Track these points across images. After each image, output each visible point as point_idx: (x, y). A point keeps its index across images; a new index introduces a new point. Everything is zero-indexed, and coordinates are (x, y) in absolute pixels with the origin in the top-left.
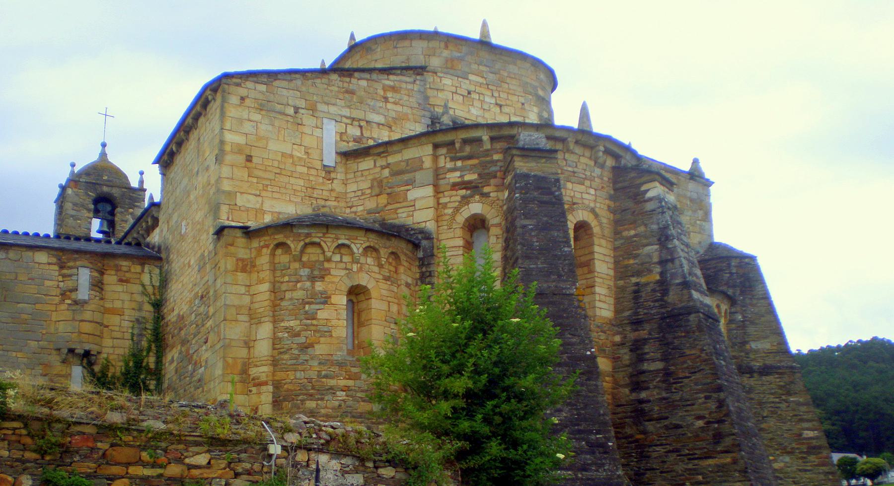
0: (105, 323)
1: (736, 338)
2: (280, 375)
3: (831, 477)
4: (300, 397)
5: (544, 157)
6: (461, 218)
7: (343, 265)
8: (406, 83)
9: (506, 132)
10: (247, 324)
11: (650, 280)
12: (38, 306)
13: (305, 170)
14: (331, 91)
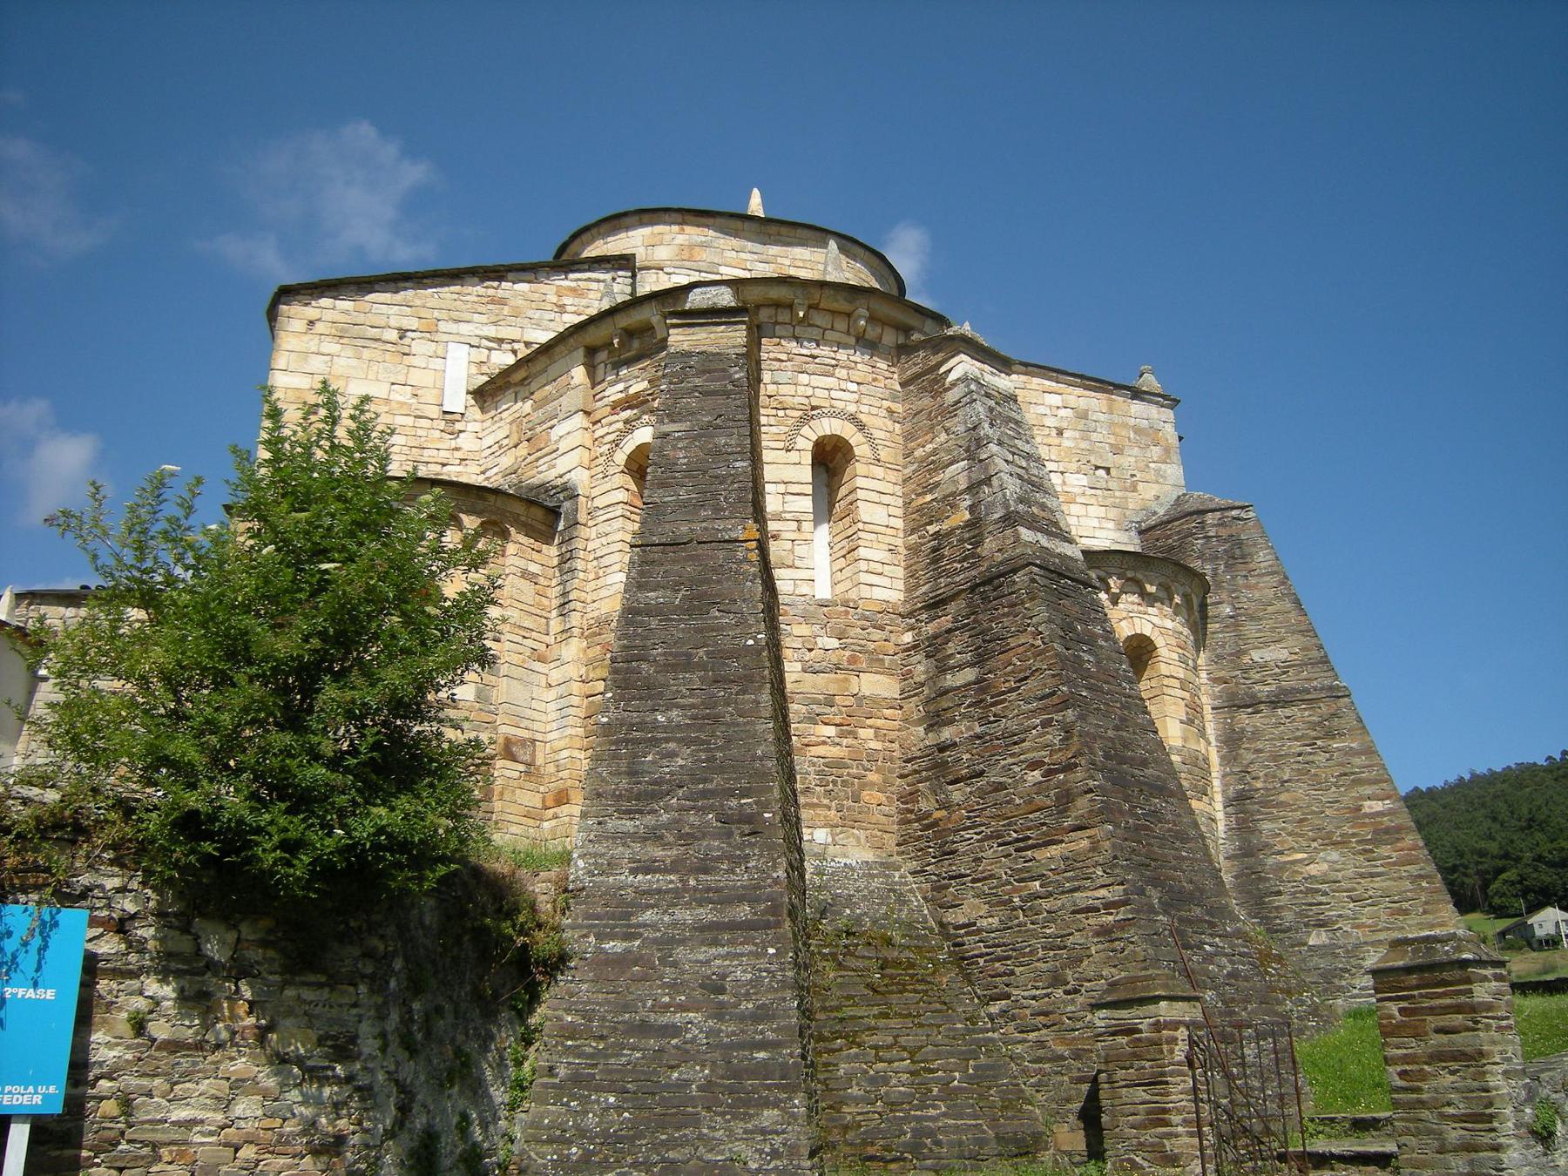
1: (1223, 647)
6: (621, 457)
13: (410, 421)
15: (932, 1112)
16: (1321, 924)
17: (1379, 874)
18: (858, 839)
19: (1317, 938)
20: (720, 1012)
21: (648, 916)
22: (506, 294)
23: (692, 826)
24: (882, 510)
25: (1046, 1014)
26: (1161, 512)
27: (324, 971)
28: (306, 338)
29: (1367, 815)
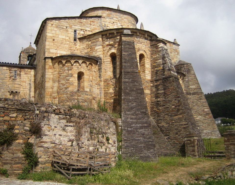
0: (21, 85)
2: (60, 96)
4: (65, 102)
6: (109, 54)
7: (77, 66)
8: (96, 20)
9: (121, 31)
10: (52, 82)
11: (160, 69)
12: (4, 80)
13: (69, 43)
20: (144, 138)
21: (133, 125)
22: (82, 21)
24: (148, 65)
25: (175, 138)
26: (177, 63)
28: (51, 27)
29: (205, 111)
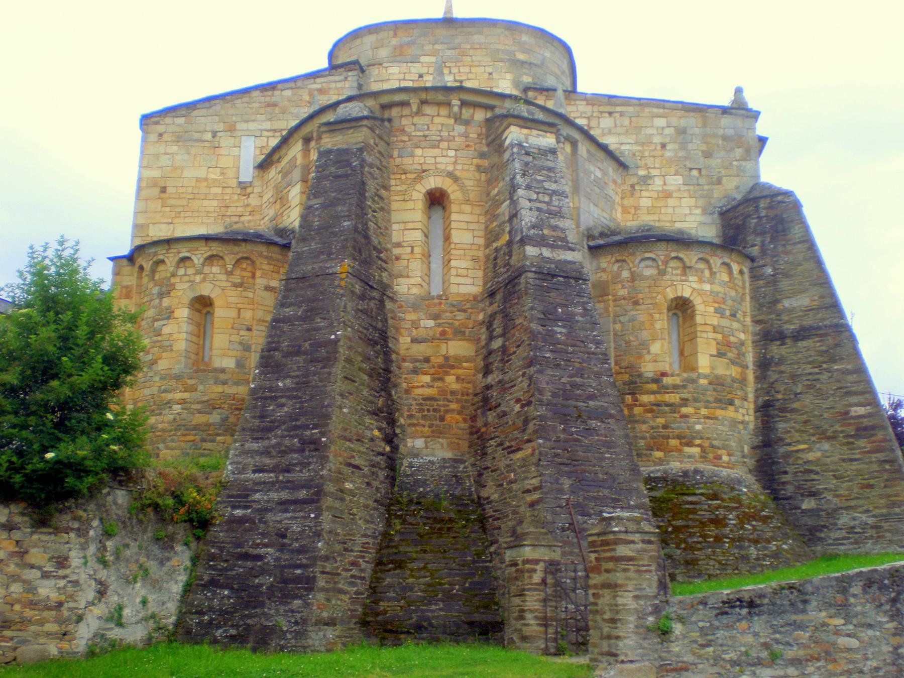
3: (887, 467)
5: (351, 128)
8: (336, 82)
13: (219, 190)
14: (252, 108)
15: (433, 607)
16: (813, 494)
17: (856, 460)
18: (442, 445)
19: (808, 504)
20: (282, 548)
21: (257, 496)
23: (286, 446)
27: (50, 527)
